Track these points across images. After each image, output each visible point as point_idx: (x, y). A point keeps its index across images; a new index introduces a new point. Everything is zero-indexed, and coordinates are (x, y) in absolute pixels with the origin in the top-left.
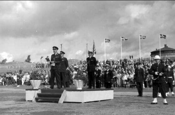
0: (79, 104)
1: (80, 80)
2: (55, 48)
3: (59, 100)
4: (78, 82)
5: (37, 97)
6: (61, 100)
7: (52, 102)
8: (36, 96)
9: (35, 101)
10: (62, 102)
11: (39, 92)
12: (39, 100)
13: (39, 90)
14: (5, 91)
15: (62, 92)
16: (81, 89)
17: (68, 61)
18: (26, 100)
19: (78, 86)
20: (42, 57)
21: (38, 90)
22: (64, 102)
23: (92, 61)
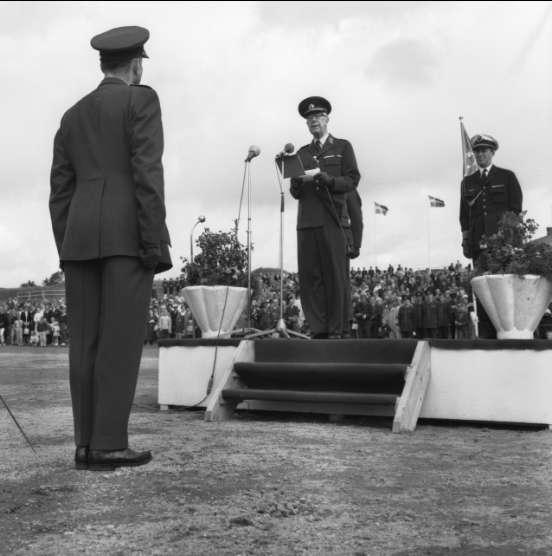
0: (532, 436)
1: (529, 277)
2: (314, 108)
3: (392, 405)
4: (518, 290)
5: (236, 387)
6: (406, 409)
7: (322, 419)
8: (223, 381)
9: (221, 413)
10: (414, 421)
11: (243, 353)
12: (240, 406)
13: (243, 343)
14: (55, 361)
15: (408, 357)
16: (527, 334)
17: (140, 372)
18: (160, 401)
19: (510, 317)
20: (253, 154)
21: (233, 342)
22: (423, 422)
23: (496, 193)
